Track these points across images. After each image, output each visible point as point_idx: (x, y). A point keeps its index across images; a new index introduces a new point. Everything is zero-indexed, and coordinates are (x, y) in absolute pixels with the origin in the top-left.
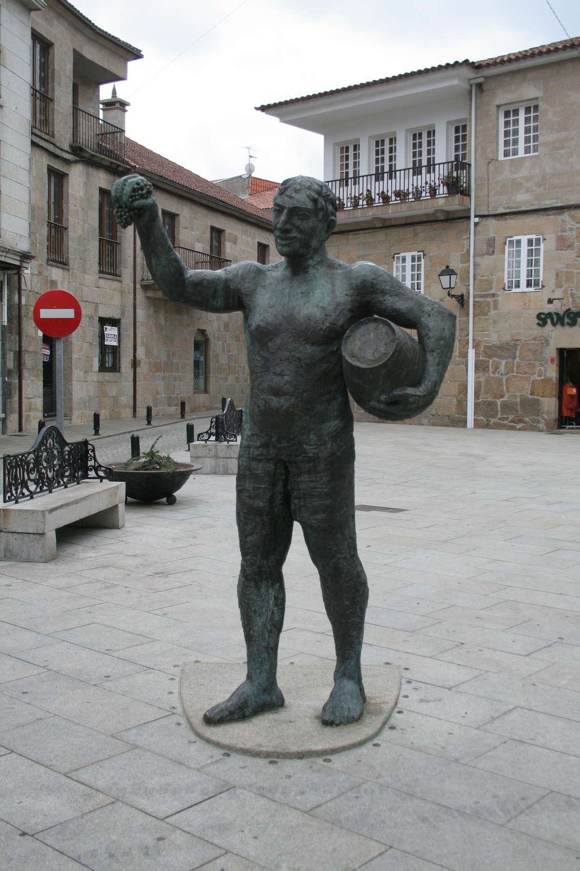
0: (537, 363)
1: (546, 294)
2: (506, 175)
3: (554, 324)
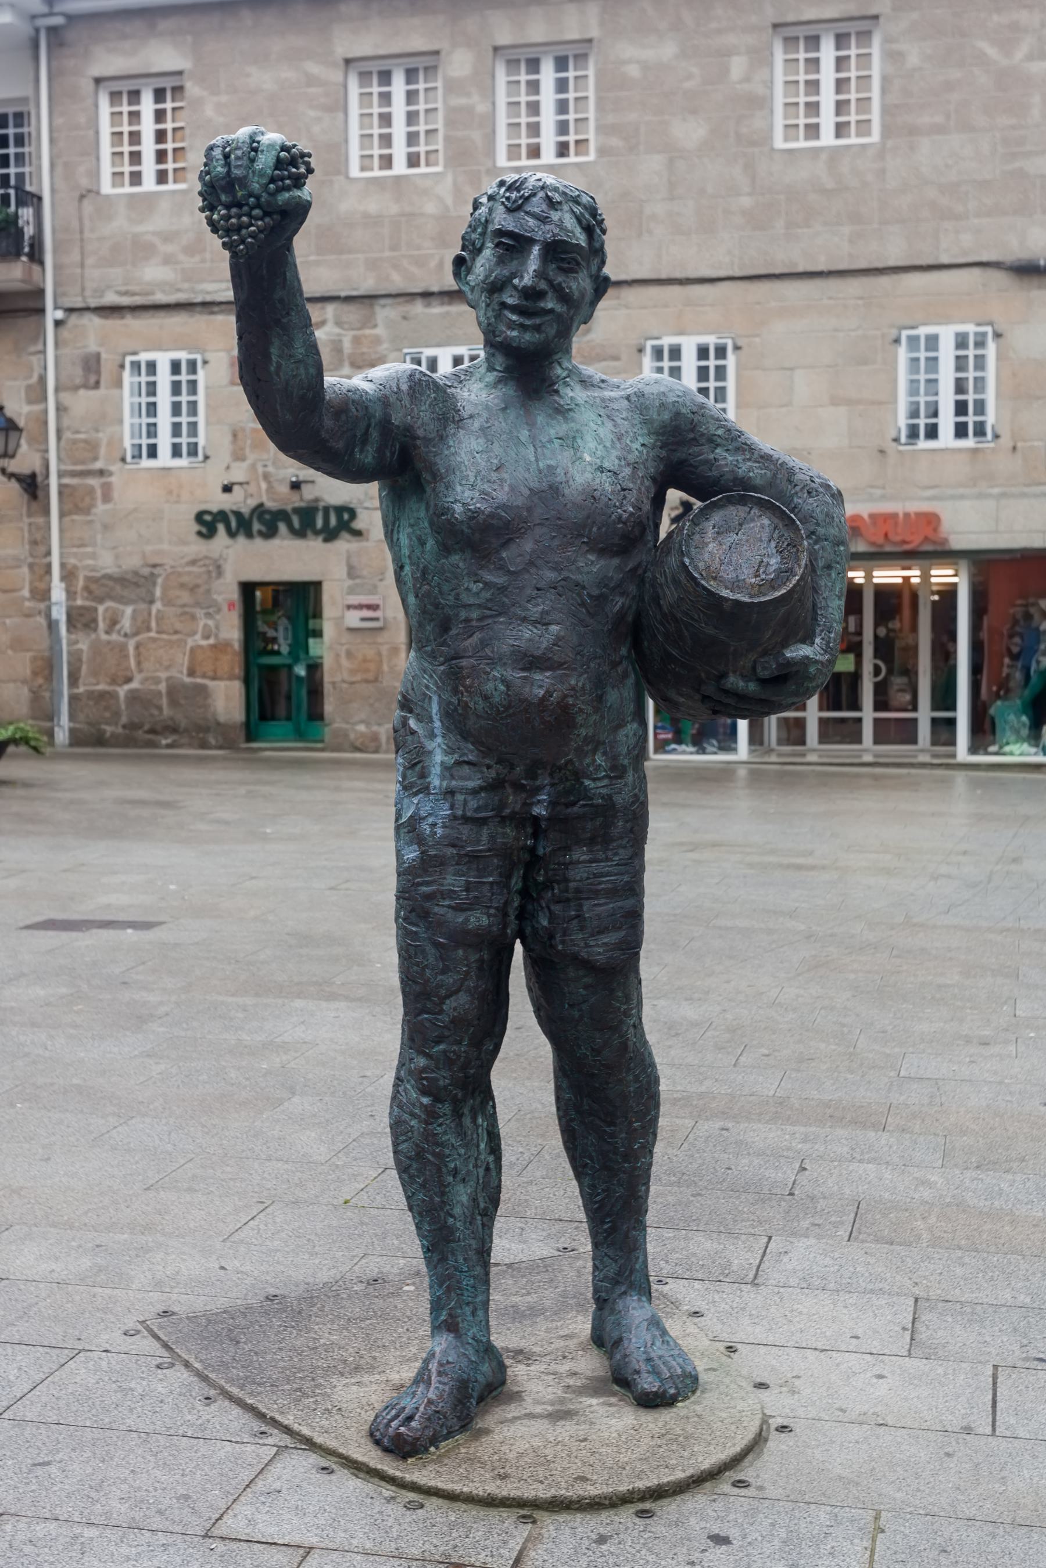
0: (200, 613)
2: (120, 224)
3: (232, 534)
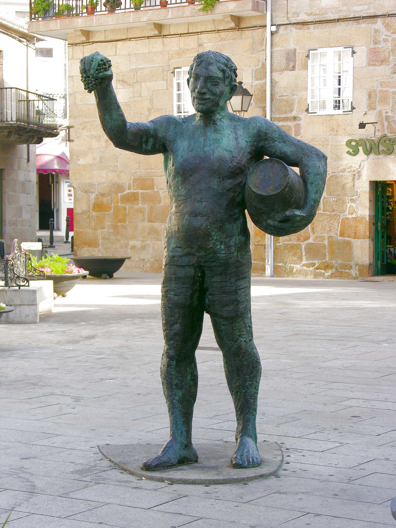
1: (358, 117)
